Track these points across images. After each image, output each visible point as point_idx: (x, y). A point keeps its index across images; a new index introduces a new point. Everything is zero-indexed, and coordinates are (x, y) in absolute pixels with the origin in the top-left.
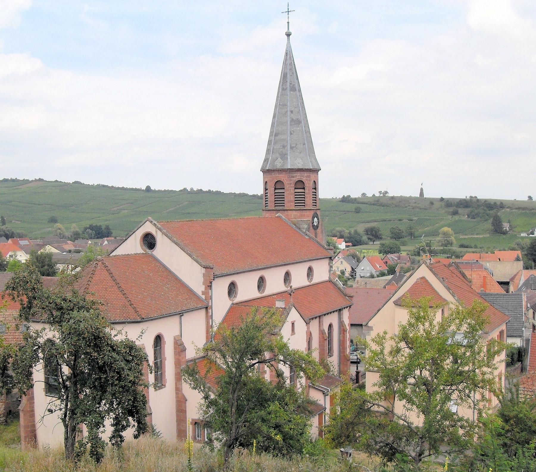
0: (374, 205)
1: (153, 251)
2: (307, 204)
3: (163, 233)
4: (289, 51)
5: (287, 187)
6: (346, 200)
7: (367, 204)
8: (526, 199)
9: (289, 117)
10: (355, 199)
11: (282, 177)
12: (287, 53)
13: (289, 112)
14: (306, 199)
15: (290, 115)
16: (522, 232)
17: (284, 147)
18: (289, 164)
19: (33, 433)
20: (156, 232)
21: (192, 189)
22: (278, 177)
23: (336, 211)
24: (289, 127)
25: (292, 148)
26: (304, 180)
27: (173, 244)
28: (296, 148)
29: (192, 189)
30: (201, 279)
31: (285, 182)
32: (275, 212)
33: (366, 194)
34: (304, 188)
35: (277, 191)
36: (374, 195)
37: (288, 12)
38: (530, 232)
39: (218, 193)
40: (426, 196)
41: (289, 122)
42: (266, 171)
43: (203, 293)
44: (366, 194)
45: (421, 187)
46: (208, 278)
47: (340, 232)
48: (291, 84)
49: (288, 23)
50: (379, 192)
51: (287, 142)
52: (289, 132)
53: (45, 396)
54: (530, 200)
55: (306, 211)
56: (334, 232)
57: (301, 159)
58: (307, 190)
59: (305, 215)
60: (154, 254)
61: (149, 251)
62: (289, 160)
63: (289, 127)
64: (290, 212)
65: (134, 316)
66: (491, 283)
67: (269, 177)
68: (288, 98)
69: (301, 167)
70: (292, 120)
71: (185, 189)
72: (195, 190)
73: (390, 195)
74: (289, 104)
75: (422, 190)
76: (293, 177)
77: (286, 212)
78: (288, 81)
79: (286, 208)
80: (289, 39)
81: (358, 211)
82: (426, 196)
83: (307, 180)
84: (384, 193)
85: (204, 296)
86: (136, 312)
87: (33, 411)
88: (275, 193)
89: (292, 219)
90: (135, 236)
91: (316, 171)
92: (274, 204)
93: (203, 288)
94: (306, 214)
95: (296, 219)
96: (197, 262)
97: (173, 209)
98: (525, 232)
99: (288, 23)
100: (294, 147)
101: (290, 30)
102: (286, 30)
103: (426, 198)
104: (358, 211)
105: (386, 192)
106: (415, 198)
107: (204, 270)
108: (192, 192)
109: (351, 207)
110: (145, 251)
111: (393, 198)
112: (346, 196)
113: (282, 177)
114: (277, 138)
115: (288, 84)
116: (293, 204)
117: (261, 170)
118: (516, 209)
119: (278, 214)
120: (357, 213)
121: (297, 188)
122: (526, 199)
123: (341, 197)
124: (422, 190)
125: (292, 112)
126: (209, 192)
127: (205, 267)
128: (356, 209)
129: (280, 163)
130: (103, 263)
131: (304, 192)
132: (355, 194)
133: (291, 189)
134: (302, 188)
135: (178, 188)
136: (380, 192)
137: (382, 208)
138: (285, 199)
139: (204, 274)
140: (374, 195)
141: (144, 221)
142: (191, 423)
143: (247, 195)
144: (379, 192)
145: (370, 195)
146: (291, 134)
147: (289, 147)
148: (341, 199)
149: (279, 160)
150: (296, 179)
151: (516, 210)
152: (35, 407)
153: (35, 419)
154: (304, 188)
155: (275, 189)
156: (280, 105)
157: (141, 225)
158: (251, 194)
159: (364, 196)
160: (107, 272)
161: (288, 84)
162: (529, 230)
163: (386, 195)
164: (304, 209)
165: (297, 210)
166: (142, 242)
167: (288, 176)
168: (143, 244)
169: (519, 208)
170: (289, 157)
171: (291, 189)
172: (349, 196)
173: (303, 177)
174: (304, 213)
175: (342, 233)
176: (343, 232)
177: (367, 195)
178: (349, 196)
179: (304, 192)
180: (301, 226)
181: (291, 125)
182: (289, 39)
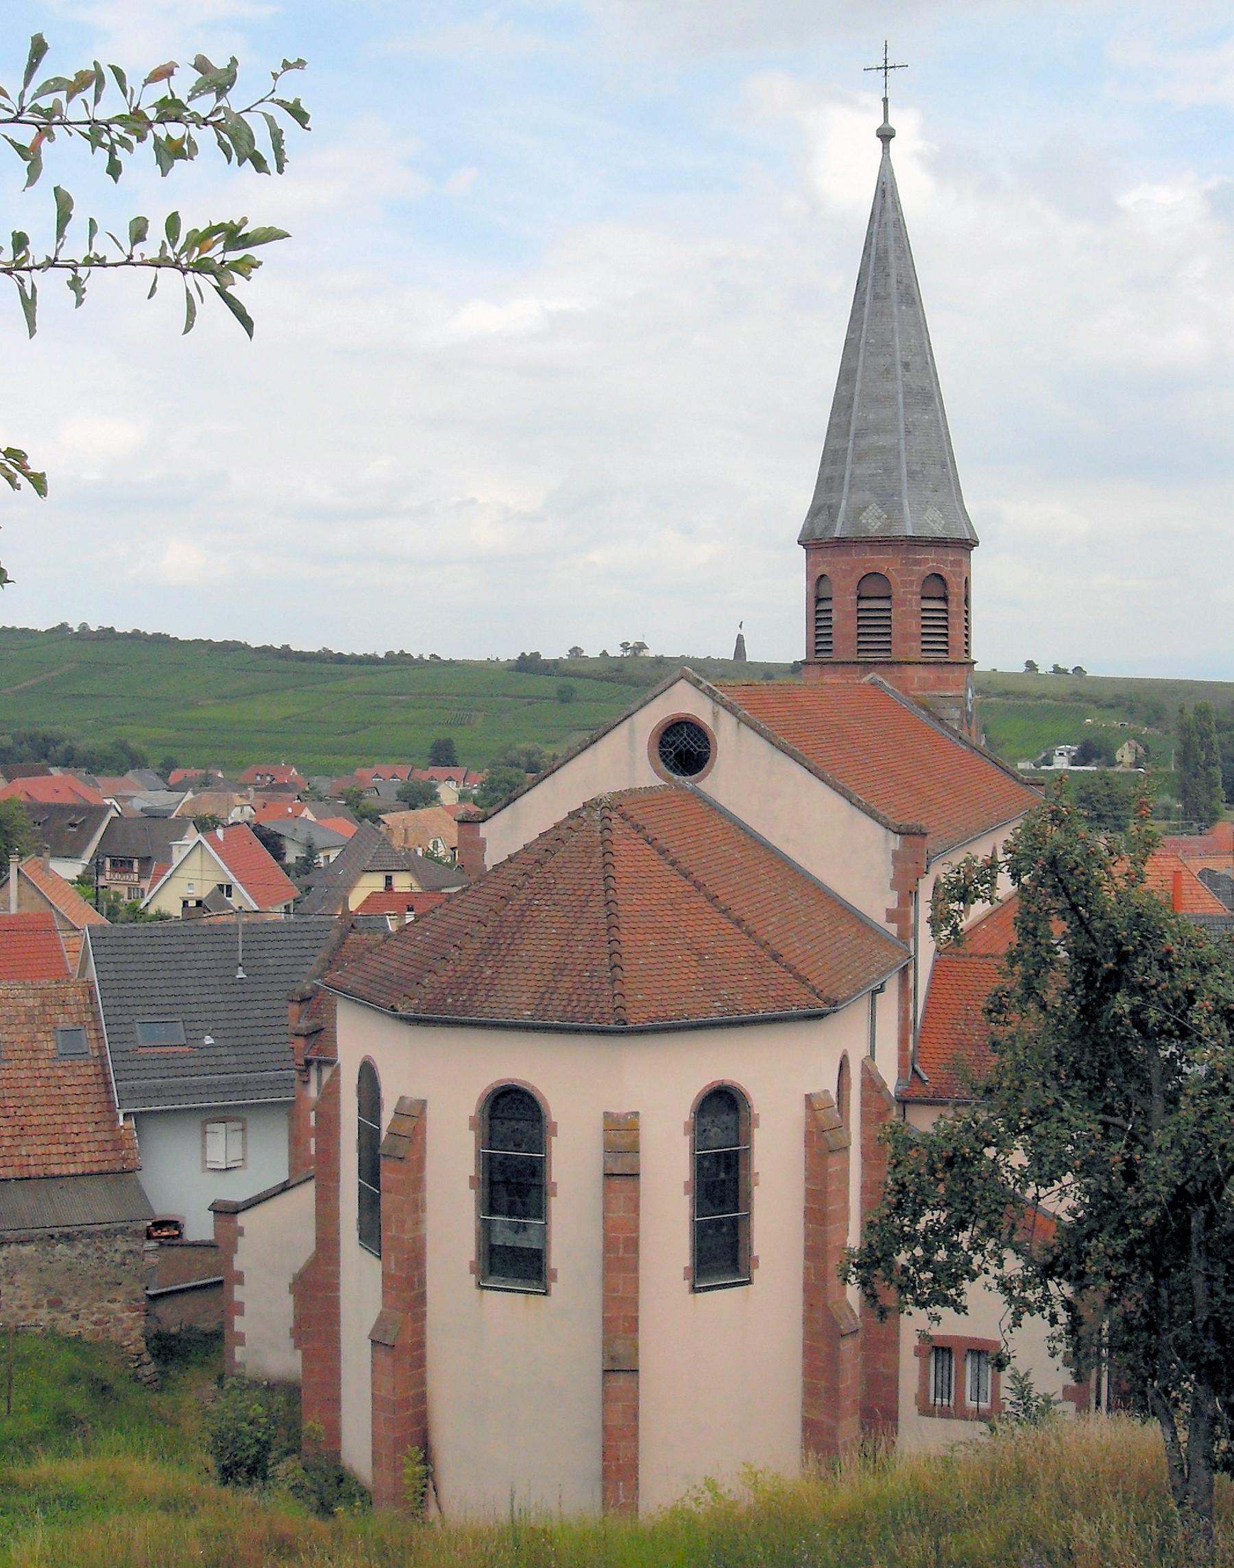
0: (608, 679)
1: (698, 780)
2: (953, 646)
3: (741, 720)
4: (889, 186)
5: (898, 592)
6: (529, 664)
7: (588, 677)
8: (1021, 668)
9: (900, 382)
10: (556, 663)
11: (885, 562)
12: (884, 191)
13: (899, 368)
14: (950, 632)
15: (904, 376)
16: (1022, 757)
17: (887, 470)
18: (909, 524)
19: (419, 1424)
20: (715, 715)
21: (84, 627)
22: (868, 561)
23: (505, 695)
24: (902, 411)
25: (912, 475)
26: (946, 571)
27: (780, 756)
28: (924, 476)
29: (84, 627)
30: (884, 870)
31: (895, 578)
32: (859, 668)
33: (582, 651)
34: (945, 599)
35: (865, 604)
36: (604, 654)
37: (886, 68)
38: (1040, 758)
39: (161, 640)
40: (751, 657)
41: (900, 396)
42: (812, 543)
43: (891, 916)
44: (582, 651)
45: (739, 631)
46: (911, 866)
47: (529, 755)
48: (899, 282)
49: (885, 100)
50: (622, 646)
51: (898, 457)
52: (902, 426)
53: (478, 1291)
54: (1029, 674)
55: (950, 667)
56: (513, 754)
57: (939, 509)
58: (954, 605)
59: (948, 678)
60: (704, 789)
61: (686, 781)
62: (907, 510)
63: (902, 411)
64: (910, 670)
65: (800, 999)
66: (1194, 892)
67: (831, 564)
68: (896, 324)
69: (941, 534)
70: (908, 392)
71: (63, 627)
72: (94, 628)
73: (652, 653)
74: (897, 341)
75: (740, 640)
76: (918, 562)
77: (896, 668)
78: (893, 273)
79: (894, 657)
80: (886, 149)
81: (565, 696)
82: (751, 657)
83: (954, 573)
84: (634, 648)
85: (895, 925)
86: (803, 980)
87: (420, 1345)
88: (859, 610)
89: (913, 690)
90: (632, 731)
91: (968, 544)
92: (856, 644)
93: (891, 900)
94: (951, 676)
95: (925, 690)
96: (871, 814)
97: (33, 681)
98: (1028, 757)
99: (885, 100)
100: (917, 472)
101: (892, 123)
102: (879, 122)
103: (751, 663)
104: (565, 696)
105: (642, 646)
106: (723, 663)
107: (895, 842)
108: (85, 634)
109: (549, 685)
110: (668, 779)
111: (660, 660)
112: (528, 654)
113: (885, 562)
114: (863, 443)
115: (893, 281)
116: (917, 645)
117: (799, 542)
118: (999, 695)
119: (870, 676)
120: (563, 701)
121: (929, 598)
122: (1021, 668)
123: (515, 656)
124: (740, 640)
125: (906, 366)
126: (136, 635)
127: (903, 829)
128: (560, 692)
129: (878, 518)
130: (622, 816)
131: (945, 611)
132: (553, 650)
133: (911, 599)
134: (939, 598)
135: (42, 623)
136: (625, 646)
137: (633, 689)
138: (894, 631)
139: (896, 856)
140: (604, 654)
141: (669, 681)
142: (918, 1351)
143: (244, 647)
144: (622, 646)
145: (592, 652)
146: (908, 432)
147: (904, 471)
148: (513, 664)
149: (874, 509)
150: (926, 569)
151: (998, 699)
152: (428, 1332)
153: (425, 1372)
154: (945, 599)
155: (860, 598)
156: (867, 343)
157: (657, 692)
158: (255, 643)
159: (577, 655)
160: (649, 847)
161: (893, 281)
162: (1039, 753)
163: (642, 654)
164: (948, 660)
165: (929, 663)
166: (656, 750)
167: (903, 559)
168: (657, 756)
169: (1006, 694)
170: (906, 502)
171: (911, 599)
172: (537, 655)
173: (944, 562)
174: (947, 673)
175: (535, 758)
176: (537, 755)
177: (584, 654)
178: (537, 655)
179: (945, 611)
180: (945, 714)
181: (906, 405)
182: (886, 149)
